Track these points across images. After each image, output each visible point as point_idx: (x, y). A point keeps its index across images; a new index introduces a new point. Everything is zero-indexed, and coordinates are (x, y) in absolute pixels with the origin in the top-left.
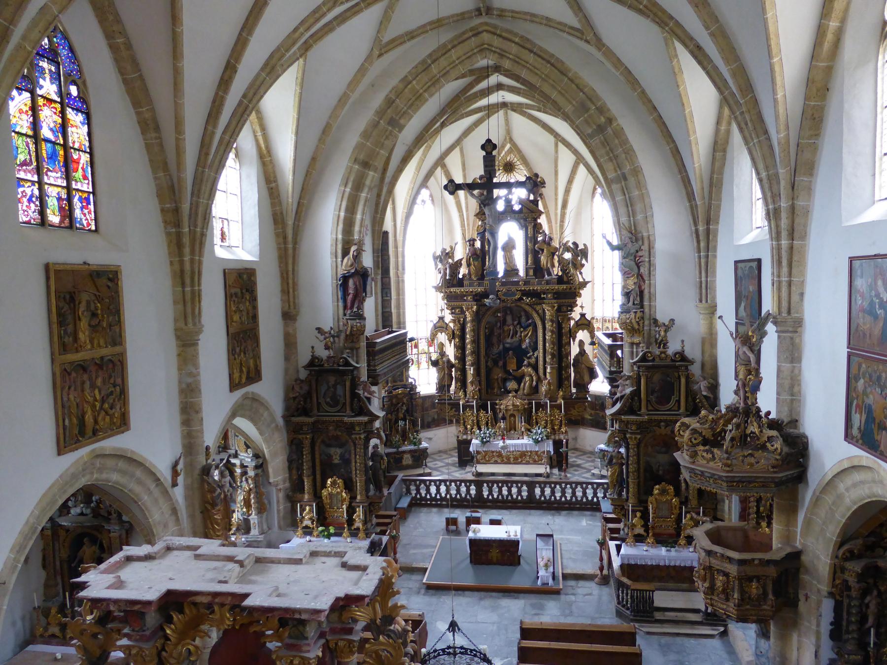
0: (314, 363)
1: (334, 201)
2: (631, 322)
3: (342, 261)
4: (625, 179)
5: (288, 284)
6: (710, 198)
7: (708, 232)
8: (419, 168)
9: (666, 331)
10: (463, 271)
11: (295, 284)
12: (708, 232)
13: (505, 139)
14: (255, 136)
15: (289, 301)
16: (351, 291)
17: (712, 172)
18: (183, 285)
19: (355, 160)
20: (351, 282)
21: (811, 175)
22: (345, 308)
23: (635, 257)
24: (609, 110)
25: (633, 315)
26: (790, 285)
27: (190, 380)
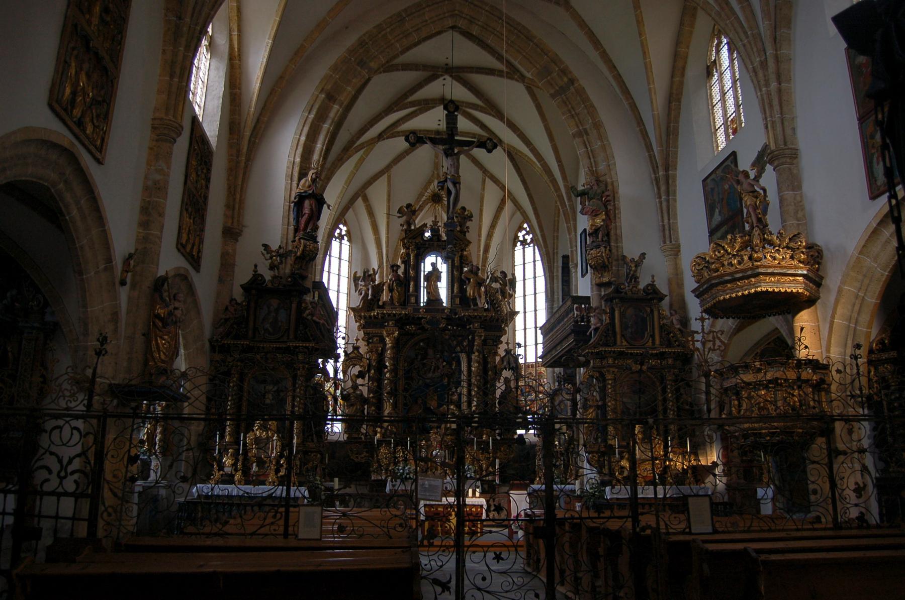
0: (255, 286)
1: (294, 130)
2: (601, 256)
3: (298, 185)
4: (587, 134)
5: (234, 200)
6: (668, 147)
7: (667, 178)
8: (348, 182)
9: (636, 266)
10: (385, 297)
11: (242, 202)
12: (667, 178)
13: (433, 175)
14: (231, 35)
15: (233, 218)
16: (306, 211)
17: (669, 123)
18: (172, 76)
19: (323, 89)
20: (307, 203)
21: (789, 28)
22: (296, 230)
23: (602, 197)
24: (571, 72)
25: (603, 249)
26: (783, 123)
27: (158, 177)
